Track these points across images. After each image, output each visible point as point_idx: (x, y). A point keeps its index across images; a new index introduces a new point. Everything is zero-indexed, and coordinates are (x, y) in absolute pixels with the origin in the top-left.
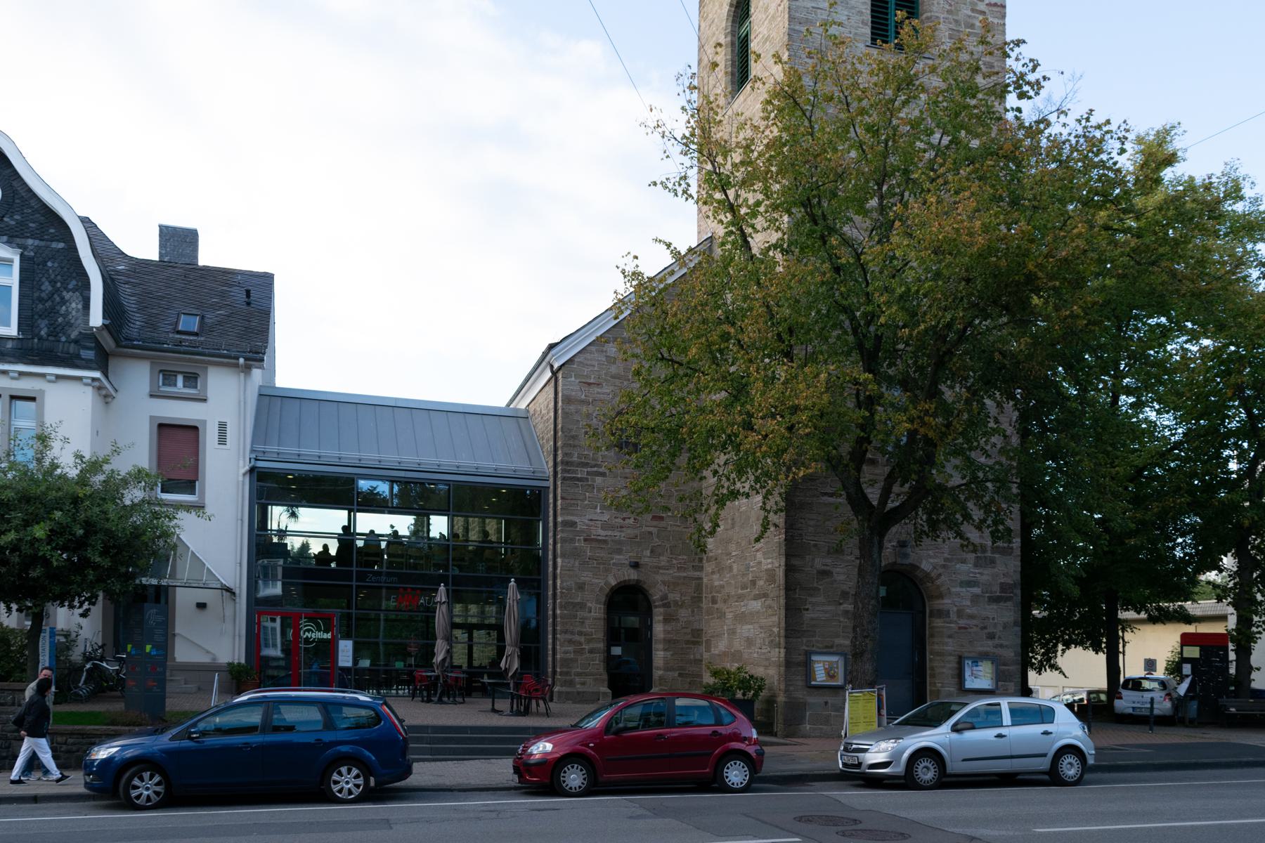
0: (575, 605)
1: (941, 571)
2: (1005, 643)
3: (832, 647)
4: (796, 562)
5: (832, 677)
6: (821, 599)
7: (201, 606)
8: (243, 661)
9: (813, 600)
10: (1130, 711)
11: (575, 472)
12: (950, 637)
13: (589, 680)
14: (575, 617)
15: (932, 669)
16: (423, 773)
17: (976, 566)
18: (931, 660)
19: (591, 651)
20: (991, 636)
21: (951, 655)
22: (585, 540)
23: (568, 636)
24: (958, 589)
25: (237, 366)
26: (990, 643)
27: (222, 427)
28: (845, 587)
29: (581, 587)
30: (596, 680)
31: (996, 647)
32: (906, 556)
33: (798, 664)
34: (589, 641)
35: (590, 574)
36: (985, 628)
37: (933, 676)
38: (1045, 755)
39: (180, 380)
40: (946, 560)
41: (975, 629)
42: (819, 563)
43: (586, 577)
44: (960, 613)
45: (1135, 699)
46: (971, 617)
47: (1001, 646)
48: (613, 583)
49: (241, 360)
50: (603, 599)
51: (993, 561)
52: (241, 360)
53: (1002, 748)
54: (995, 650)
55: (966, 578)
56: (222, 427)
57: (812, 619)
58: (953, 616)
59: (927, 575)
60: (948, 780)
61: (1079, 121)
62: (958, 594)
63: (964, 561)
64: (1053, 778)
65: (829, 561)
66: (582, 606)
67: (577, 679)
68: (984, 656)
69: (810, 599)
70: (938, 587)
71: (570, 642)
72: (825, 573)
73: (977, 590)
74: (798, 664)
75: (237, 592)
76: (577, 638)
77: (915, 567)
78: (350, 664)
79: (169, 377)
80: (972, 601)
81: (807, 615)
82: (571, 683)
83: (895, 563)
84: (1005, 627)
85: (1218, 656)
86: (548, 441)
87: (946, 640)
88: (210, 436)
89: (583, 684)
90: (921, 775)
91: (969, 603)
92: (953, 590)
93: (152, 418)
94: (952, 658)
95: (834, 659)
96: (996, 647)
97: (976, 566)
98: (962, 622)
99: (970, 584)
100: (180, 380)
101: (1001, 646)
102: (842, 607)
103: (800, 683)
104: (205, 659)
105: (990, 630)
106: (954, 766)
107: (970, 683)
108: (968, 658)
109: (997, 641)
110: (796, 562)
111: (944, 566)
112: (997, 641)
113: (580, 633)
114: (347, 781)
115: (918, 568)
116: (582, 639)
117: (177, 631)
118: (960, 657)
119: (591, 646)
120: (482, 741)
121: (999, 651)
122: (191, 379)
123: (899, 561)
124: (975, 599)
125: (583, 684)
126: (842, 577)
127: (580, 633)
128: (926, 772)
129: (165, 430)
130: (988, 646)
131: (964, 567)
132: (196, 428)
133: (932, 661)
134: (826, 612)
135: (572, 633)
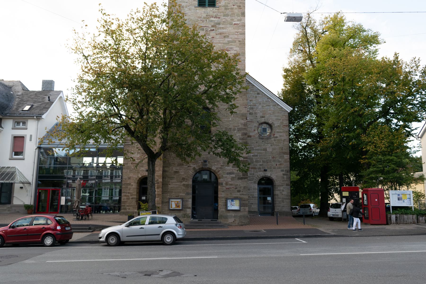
0: (127, 184)
1: (219, 169)
2: (244, 193)
3: (178, 196)
4: (166, 169)
5: (178, 206)
6: (175, 181)
7: (21, 188)
8: (32, 203)
9: (172, 181)
10: (332, 216)
11: (128, 143)
12: (223, 192)
13: (131, 208)
14: (127, 188)
16: (76, 237)
17: (233, 167)
19: (132, 199)
20: (239, 191)
21: (223, 198)
22: (131, 163)
23: (125, 194)
24: (226, 175)
25: (34, 119)
26: (238, 193)
27: (31, 136)
28: (184, 177)
29: (129, 178)
30: (133, 208)
31: (241, 195)
32: (206, 165)
33: (166, 202)
34: (131, 195)
35: (133, 174)
36: (237, 188)
38: (159, 235)
39: (21, 124)
42: (174, 169)
43: (131, 175)
45: (333, 211)
46: (231, 185)
47: (243, 194)
48: (140, 176)
49: (35, 117)
50: (137, 182)
52: (35, 117)
53: (142, 232)
54: (240, 196)
55: (229, 172)
56: (31, 136)
57: (171, 187)
58: (224, 185)
60: (120, 243)
62: (226, 177)
64: (161, 242)
65: (178, 168)
66: (129, 184)
67: (127, 208)
68: (236, 198)
69: (171, 181)
70: (219, 175)
71: (125, 196)
72: (176, 172)
74: (166, 202)
75: (31, 183)
76: (127, 194)
78: (64, 204)
79: (18, 123)
80: (231, 179)
81: (170, 186)
82: (125, 209)
83: (203, 168)
84: (244, 188)
85: (355, 195)
88: (27, 139)
89: (129, 209)
90: (167, 240)
91: (230, 180)
92: (224, 176)
93: (26, 135)
94: (223, 199)
95: (179, 200)
96: (241, 195)
97: (233, 167)
98: (227, 187)
99: (230, 173)
100: (21, 124)
101: (243, 194)
102: (182, 183)
103: (167, 209)
104: (21, 203)
106: (123, 239)
107: (230, 208)
108: (230, 199)
109: (241, 193)
110: (166, 169)
111: (221, 168)
112: (241, 193)
113: (129, 193)
114: (49, 241)
116: (129, 195)
117: (14, 195)
119: (132, 197)
120: (198, 226)
121: (242, 196)
122: (24, 123)
123: (204, 167)
124: (233, 179)
125: (129, 209)
126: (183, 173)
127: (129, 193)
128: (113, 240)
129: (15, 138)
130: (238, 195)
132: (24, 137)
134: (176, 185)
135: (126, 193)
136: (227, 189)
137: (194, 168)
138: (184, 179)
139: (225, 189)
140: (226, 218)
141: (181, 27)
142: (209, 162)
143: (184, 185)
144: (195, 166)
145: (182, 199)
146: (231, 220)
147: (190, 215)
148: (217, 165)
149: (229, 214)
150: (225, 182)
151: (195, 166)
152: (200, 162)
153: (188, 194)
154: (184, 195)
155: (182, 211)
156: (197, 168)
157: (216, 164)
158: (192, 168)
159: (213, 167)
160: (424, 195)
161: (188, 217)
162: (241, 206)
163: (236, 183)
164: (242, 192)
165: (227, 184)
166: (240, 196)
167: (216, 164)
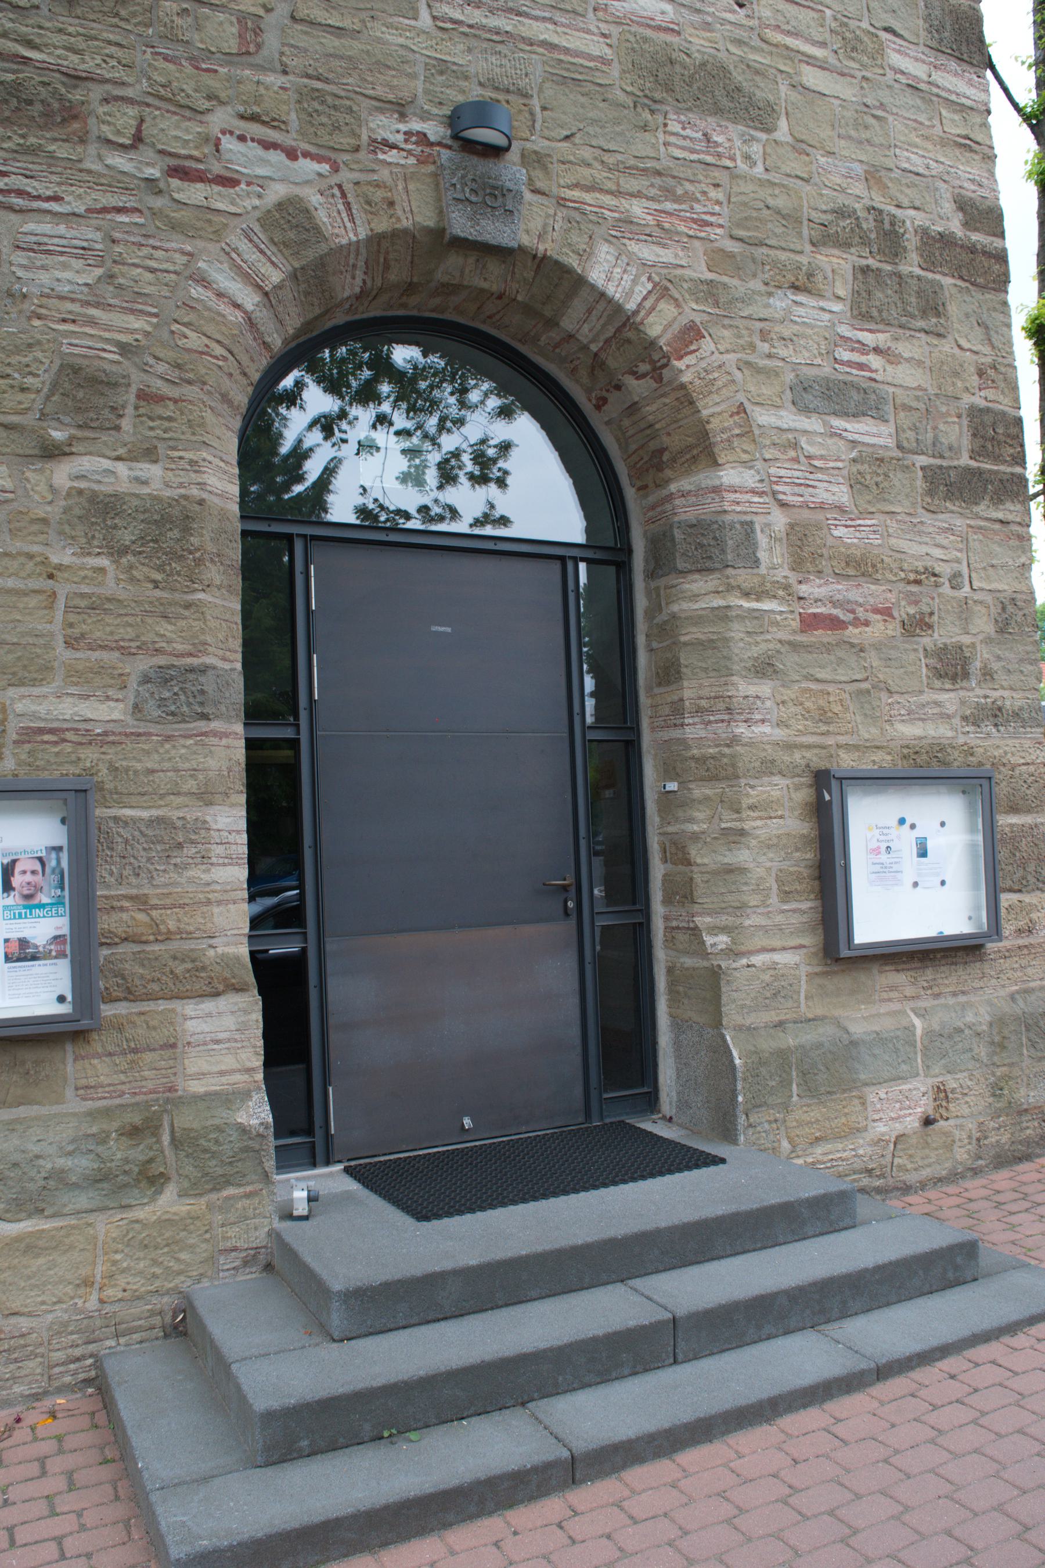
1: (694, 311)
12: (764, 668)
15: (678, 852)
18: (666, 798)
20: (952, 667)
24: (789, 419)
26: (950, 699)
28: (78, 344)
32: (495, 198)
37: (682, 893)
40: (718, 259)
41: (878, 630)
44: (804, 547)
46: (861, 567)
47: (996, 714)
51: (932, 306)
54: (971, 737)
58: (772, 557)
59: (623, 325)
61: (356, 418)
63: (803, 284)
73: (873, 433)
77: (560, 280)
80: (856, 484)
86: (54, 1295)
87: (744, 688)
91: (842, 494)
92: (763, 417)
101: (996, 714)
105: (946, 633)
109: (976, 693)
111: (709, 291)
112: (976, 693)
115: (580, 282)
118: (822, 779)
124: (870, 474)
130: (929, 718)
131: (808, 310)
133: (676, 817)
136: (810, 622)
137: (289, 222)
138: (87, 394)
139: (789, 628)
140: (832, 1073)
141: (85, 577)
142: (536, 160)
143: (100, 510)
144: (301, 179)
145: (75, 801)
146: (893, 1110)
147: (257, 1113)
148: (661, 236)
149: (876, 1012)
150: (779, 520)
151: (301, 179)
152: (386, 126)
153: (174, 690)
154: (107, 712)
155: (70, 1065)
156: (343, 228)
157: (637, 209)
158: (245, 202)
159: (604, 252)
160: (8, 959)
161: (213, 1165)
162: (1001, 868)
163: (917, 550)
164: (988, 674)
165: (804, 547)
166: (971, 737)
167: (637, 209)
